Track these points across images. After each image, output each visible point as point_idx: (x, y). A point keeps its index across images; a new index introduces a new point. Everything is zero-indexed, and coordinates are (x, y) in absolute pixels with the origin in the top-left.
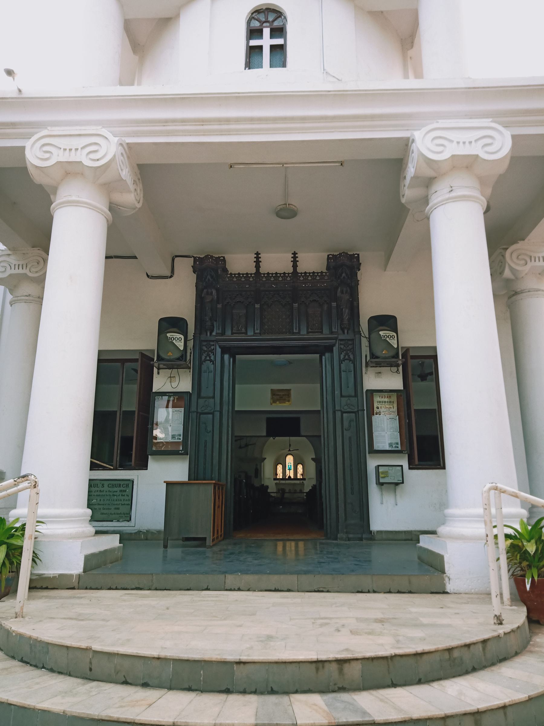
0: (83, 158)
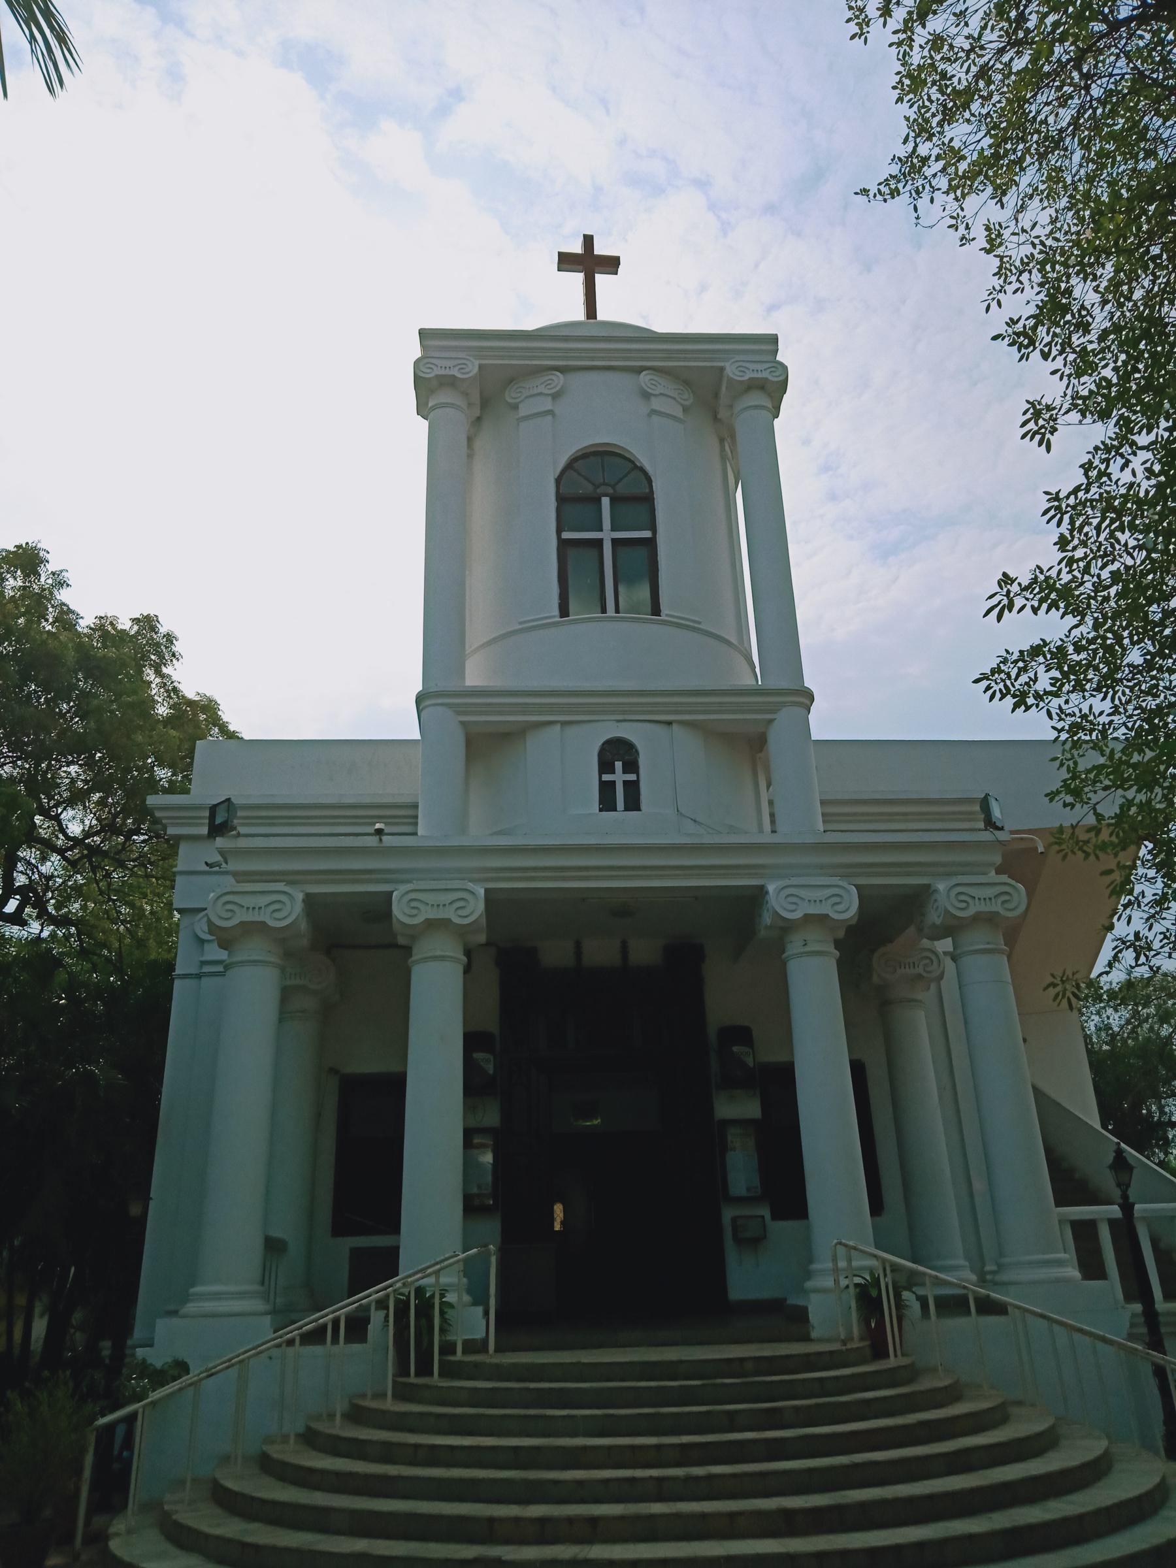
0: (450, 914)
